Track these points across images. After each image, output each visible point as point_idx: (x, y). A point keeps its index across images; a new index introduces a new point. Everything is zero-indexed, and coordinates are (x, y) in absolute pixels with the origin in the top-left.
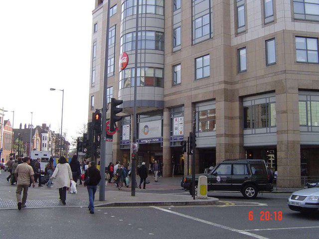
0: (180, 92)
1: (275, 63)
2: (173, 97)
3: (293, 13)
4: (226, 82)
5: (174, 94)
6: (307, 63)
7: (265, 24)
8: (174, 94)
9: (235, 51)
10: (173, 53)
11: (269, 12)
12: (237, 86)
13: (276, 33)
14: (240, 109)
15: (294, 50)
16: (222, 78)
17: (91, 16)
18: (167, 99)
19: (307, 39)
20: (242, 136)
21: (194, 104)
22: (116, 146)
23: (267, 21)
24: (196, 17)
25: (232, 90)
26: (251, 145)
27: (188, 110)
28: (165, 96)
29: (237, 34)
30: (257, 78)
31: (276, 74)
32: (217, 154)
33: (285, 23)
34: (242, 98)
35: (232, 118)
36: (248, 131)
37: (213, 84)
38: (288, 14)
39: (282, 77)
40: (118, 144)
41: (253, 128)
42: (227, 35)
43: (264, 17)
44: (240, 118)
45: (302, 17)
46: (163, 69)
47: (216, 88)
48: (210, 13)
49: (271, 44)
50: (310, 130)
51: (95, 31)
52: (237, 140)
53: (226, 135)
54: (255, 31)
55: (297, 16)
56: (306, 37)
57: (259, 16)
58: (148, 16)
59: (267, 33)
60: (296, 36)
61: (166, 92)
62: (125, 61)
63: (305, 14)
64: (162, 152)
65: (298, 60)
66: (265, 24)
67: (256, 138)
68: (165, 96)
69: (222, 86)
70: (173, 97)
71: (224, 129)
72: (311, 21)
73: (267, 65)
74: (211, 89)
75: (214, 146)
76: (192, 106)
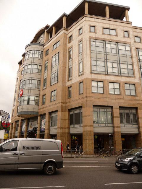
0: (45, 107)
1: (82, 93)
2: (42, 110)
3: (91, 70)
4: (62, 102)
5: (42, 108)
6: (114, 94)
7: (79, 76)
8: (42, 108)
9: (67, 88)
10: (43, 89)
11: (81, 70)
12: (67, 104)
13: (83, 80)
14: (68, 115)
15: (108, 88)
16: (60, 101)
17: (16, 74)
18: (39, 111)
19: (98, 82)
20: (69, 128)
21: (50, 113)
22: (19, 134)
23: (80, 74)
24: (53, 73)
25: (65, 106)
26: (53, 133)
27: (47, 116)
28: (39, 109)
29: (69, 81)
30: (75, 100)
31: (83, 98)
32: (83, 137)
33: (87, 75)
34: (70, 110)
35: (65, 120)
36: (72, 126)
37: (57, 104)
38: (89, 71)
39: (85, 99)
40: (20, 132)
41: (80, 123)
42: (64, 81)
43: (79, 72)
44: (68, 120)
45: (96, 72)
46: (39, 97)
47: (58, 105)
48: (58, 71)
49: (81, 84)
50: (106, 126)
51: (17, 81)
52: (67, 131)
53: (61, 128)
54: (75, 79)
55: (93, 72)
56: (114, 83)
57: (77, 72)
58: (33, 73)
59: (80, 80)
60: (109, 82)
61: (40, 107)
62: (22, 93)
63: (97, 71)
64: (121, 135)
65: (110, 93)
66: (79, 76)
67: (76, 129)
68: (39, 109)
69: (61, 104)
70: (42, 110)
71: (60, 125)
72: (100, 74)
73: (80, 94)
74: (56, 106)
75: (81, 132)
76: (49, 114)
